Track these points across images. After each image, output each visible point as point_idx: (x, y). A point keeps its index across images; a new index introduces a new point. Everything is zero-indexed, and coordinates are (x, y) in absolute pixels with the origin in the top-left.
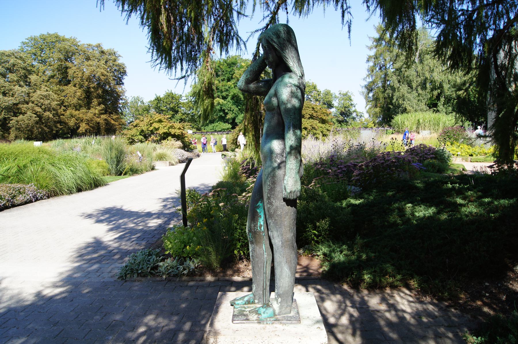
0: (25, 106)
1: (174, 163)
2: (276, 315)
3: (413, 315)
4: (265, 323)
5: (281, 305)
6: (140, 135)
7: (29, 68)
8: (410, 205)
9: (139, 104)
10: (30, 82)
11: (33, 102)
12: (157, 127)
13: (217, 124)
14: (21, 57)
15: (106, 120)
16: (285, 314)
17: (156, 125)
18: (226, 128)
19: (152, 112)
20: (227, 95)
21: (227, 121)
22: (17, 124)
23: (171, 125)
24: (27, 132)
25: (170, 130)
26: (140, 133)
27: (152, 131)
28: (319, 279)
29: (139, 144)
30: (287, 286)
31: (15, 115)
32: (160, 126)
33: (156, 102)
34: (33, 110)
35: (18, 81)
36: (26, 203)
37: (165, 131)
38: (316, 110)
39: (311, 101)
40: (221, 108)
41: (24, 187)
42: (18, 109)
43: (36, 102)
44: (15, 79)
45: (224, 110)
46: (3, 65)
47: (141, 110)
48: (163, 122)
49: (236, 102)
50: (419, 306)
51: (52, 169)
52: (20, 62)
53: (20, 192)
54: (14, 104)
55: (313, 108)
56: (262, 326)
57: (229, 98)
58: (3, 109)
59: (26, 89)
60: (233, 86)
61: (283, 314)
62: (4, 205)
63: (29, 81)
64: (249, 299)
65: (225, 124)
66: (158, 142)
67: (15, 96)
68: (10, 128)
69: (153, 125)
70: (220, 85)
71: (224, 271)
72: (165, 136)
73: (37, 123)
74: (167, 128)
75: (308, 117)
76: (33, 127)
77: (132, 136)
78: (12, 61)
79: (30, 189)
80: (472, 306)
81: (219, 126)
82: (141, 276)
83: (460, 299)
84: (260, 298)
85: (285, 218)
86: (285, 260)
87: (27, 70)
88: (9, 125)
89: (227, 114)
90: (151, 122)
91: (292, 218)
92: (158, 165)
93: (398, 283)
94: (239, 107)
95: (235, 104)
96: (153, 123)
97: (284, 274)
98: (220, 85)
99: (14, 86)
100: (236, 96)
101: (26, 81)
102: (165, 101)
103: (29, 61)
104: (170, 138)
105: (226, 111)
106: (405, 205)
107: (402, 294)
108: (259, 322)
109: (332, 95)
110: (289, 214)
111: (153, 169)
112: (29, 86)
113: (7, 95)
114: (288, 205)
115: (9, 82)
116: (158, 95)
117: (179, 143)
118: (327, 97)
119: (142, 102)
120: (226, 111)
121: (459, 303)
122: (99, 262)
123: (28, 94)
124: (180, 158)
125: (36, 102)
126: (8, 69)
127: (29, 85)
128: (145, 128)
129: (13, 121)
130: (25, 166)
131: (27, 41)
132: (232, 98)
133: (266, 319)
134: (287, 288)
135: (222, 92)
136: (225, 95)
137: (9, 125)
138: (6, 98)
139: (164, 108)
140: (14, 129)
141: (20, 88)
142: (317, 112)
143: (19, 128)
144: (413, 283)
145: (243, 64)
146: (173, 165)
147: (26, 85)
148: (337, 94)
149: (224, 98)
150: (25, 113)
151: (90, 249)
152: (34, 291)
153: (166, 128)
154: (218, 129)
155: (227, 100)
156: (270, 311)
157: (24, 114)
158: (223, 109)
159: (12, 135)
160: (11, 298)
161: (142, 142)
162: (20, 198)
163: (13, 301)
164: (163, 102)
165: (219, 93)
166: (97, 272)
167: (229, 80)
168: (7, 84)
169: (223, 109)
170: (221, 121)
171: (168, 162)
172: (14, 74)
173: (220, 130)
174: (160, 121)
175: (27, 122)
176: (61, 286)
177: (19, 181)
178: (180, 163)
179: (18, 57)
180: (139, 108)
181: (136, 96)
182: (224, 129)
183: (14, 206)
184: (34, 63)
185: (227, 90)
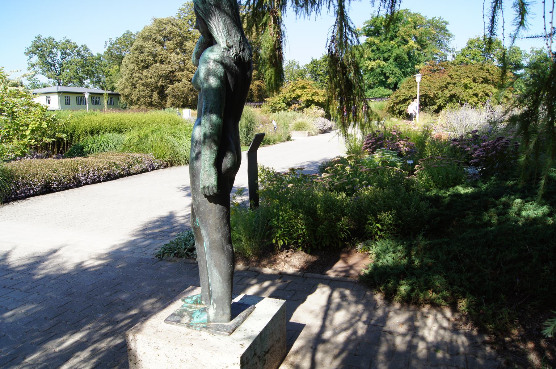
0: (180, 73)
1: (314, 133)
2: (210, 322)
3: (430, 345)
4: (194, 328)
5: (216, 311)
6: (284, 102)
7: (185, 35)
8: (519, 200)
9: (295, 68)
10: (185, 49)
11: (188, 70)
12: (299, 94)
13: (376, 89)
14: (177, 24)
15: (258, 86)
16: (221, 322)
17: (299, 92)
18: (386, 94)
19: (307, 77)
20: (389, 56)
21: (388, 87)
22: (173, 92)
23: (314, 91)
24: (182, 99)
25: (313, 97)
26: (283, 100)
27: (294, 98)
28: (355, 283)
29: (282, 113)
30: (220, 291)
31: (172, 82)
32: (304, 92)
33: (311, 66)
34: (187, 76)
35: (174, 49)
36: (142, 172)
37: (308, 98)
38: (492, 72)
39: (494, 61)
40: (382, 71)
41: (142, 157)
42: (175, 76)
43: (191, 69)
44: (172, 46)
45: (385, 74)
46: (161, 33)
47: (296, 75)
48: (306, 88)
49: (399, 64)
50: (447, 336)
51: (172, 138)
52: (176, 29)
53: (137, 162)
54: (171, 72)
55: (488, 70)
56: (189, 330)
57: (391, 60)
58: (161, 77)
59: (181, 56)
60: (396, 46)
61: (218, 322)
62: (118, 173)
63: (184, 48)
64: (197, 299)
65: (385, 90)
66: (302, 109)
67: (172, 63)
68: (167, 95)
69: (296, 92)
70: (382, 44)
71: (258, 262)
72: (309, 103)
73: (191, 90)
74: (310, 94)
75: (480, 81)
76: (187, 95)
77: (275, 104)
78: (169, 28)
79: (147, 158)
80: (518, 347)
81: (378, 93)
82: (177, 257)
83: (509, 334)
84: (206, 300)
85: (209, 216)
86: (213, 264)
87: (184, 37)
88: (166, 92)
89: (388, 77)
90: (294, 88)
91: (217, 217)
92: (295, 135)
93: (441, 301)
94: (403, 70)
95: (398, 67)
96: (295, 90)
97: (214, 279)
98: (382, 44)
99: (171, 53)
100: (399, 57)
101: (182, 48)
102: (322, 64)
103: (186, 28)
104: (313, 106)
105: (388, 74)
106: (515, 199)
107: (439, 316)
108: (189, 326)
109: (521, 53)
110: (213, 212)
111: (288, 139)
112: (185, 52)
113: (165, 63)
114: (210, 202)
115: (167, 50)
116: (314, 58)
117: (322, 112)
118: (514, 55)
119: (298, 66)
120: (388, 74)
121: (504, 341)
122: (153, 238)
123: (184, 61)
124: (321, 128)
125: (191, 69)
126: (165, 37)
127: (184, 51)
128: (287, 95)
129: (169, 89)
130: (146, 136)
131: (184, 7)
132: (396, 60)
133: (197, 324)
134: (220, 295)
135: (383, 52)
136: (387, 57)
137: (166, 92)
138: (163, 66)
139: (320, 73)
140: (170, 96)
141: (176, 55)
142: (492, 75)
143: (175, 96)
144: (463, 304)
145: (409, 19)
146: (312, 135)
147: (182, 52)
148: (528, 52)
149: (386, 60)
150: (181, 80)
151: (158, 223)
152: (77, 260)
153: (309, 95)
154: (377, 95)
155: (389, 62)
156: (204, 317)
157: (179, 81)
158: (383, 72)
159: (169, 102)
160: (54, 266)
161: (285, 110)
162: (136, 168)
163: (56, 268)
164: (320, 65)
165: (380, 55)
166: (145, 247)
167: (392, 39)
168: (164, 52)
169: (383, 72)
170: (382, 86)
171: (307, 132)
172: (171, 42)
173: (380, 96)
174: (303, 88)
175: (182, 89)
176: (103, 259)
177: (140, 150)
178: (320, 133)
179: (175, 24)
180: (294, 73)
181: (291, 60)
182: (384, 96)
183: (129, 174)
184: (190, 29)
185: (389, 51)
